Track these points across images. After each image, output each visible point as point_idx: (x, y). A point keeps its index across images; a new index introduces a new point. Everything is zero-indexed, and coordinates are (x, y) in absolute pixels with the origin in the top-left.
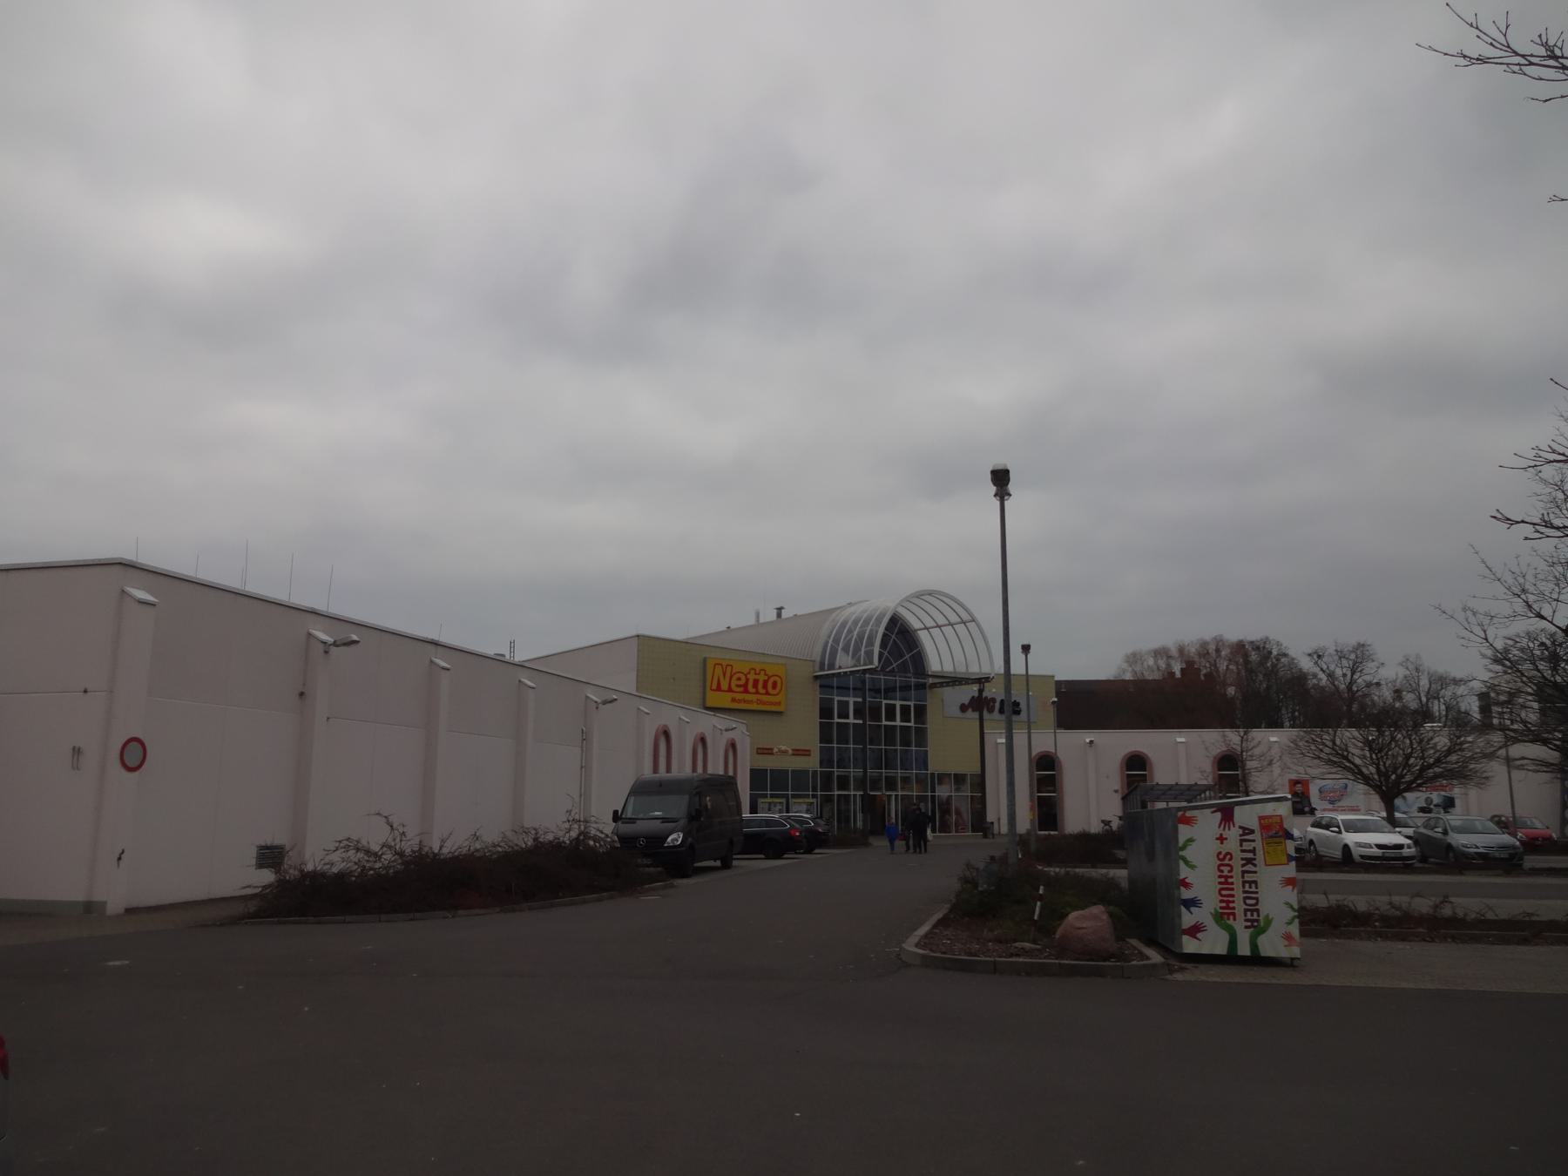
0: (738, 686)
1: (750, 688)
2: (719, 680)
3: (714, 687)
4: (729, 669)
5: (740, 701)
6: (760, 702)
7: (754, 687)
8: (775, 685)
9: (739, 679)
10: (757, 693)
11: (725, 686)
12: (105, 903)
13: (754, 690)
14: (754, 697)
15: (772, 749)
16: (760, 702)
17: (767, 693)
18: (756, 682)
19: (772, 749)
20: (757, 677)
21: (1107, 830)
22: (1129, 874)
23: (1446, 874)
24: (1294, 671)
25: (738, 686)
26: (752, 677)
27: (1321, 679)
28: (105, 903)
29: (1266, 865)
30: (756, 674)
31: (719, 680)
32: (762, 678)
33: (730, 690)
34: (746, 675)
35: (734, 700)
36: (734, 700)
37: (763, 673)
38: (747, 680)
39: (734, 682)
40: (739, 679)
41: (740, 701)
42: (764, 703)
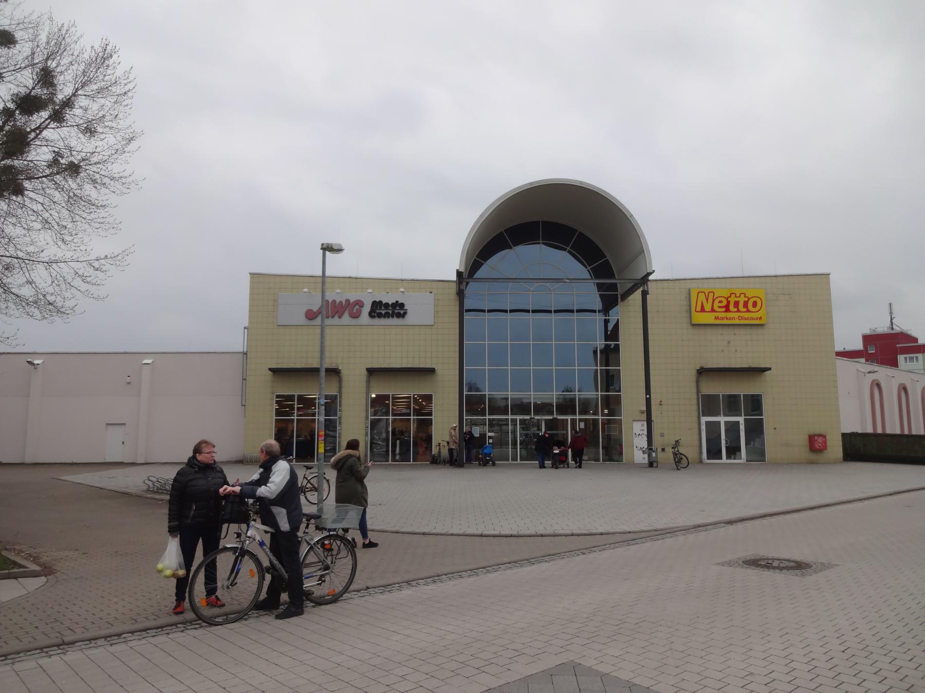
0: (720, 307)
1: (732, 308)
2: (707, 300)
3: (699, 308)
4: (711, 295)
5: (723, 319)
6: (740, 318)
7: (734, 307)
8: (755, 304)
9: (721, 302)
10: (738, 311)
11: (708, 307)
12: (825, 277)
13: (745, 310)
14: (736, 315)
15: (308, 528)
16: (740, 318)
17: (748, 311)
18: (736, 304)
19: (308, 528)
20: (737, 299)
21: (11, 165)
22: (241, 490)
23: (471, 240)
24: (18, 123)
25: (720, 307)
26: (732, 300)
27: (10, 123)
28: (825, 277)
29: (696, 311)
30: (736, 297)
31: (707, 300)
32: (742, 300)
33: (713, 310)
34: (727, 299)
35: (717, 318)
36: (717, 318)
37: (742, 296)
38: (728, 303)
39: (716, 305)
40: (721, 302)
41: (723, 319)
42: (746, 319)
